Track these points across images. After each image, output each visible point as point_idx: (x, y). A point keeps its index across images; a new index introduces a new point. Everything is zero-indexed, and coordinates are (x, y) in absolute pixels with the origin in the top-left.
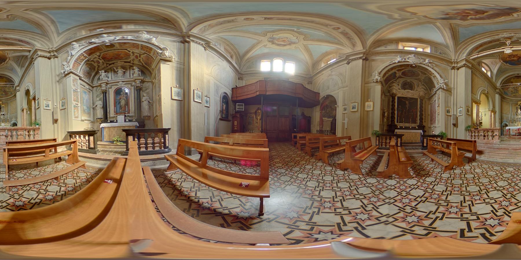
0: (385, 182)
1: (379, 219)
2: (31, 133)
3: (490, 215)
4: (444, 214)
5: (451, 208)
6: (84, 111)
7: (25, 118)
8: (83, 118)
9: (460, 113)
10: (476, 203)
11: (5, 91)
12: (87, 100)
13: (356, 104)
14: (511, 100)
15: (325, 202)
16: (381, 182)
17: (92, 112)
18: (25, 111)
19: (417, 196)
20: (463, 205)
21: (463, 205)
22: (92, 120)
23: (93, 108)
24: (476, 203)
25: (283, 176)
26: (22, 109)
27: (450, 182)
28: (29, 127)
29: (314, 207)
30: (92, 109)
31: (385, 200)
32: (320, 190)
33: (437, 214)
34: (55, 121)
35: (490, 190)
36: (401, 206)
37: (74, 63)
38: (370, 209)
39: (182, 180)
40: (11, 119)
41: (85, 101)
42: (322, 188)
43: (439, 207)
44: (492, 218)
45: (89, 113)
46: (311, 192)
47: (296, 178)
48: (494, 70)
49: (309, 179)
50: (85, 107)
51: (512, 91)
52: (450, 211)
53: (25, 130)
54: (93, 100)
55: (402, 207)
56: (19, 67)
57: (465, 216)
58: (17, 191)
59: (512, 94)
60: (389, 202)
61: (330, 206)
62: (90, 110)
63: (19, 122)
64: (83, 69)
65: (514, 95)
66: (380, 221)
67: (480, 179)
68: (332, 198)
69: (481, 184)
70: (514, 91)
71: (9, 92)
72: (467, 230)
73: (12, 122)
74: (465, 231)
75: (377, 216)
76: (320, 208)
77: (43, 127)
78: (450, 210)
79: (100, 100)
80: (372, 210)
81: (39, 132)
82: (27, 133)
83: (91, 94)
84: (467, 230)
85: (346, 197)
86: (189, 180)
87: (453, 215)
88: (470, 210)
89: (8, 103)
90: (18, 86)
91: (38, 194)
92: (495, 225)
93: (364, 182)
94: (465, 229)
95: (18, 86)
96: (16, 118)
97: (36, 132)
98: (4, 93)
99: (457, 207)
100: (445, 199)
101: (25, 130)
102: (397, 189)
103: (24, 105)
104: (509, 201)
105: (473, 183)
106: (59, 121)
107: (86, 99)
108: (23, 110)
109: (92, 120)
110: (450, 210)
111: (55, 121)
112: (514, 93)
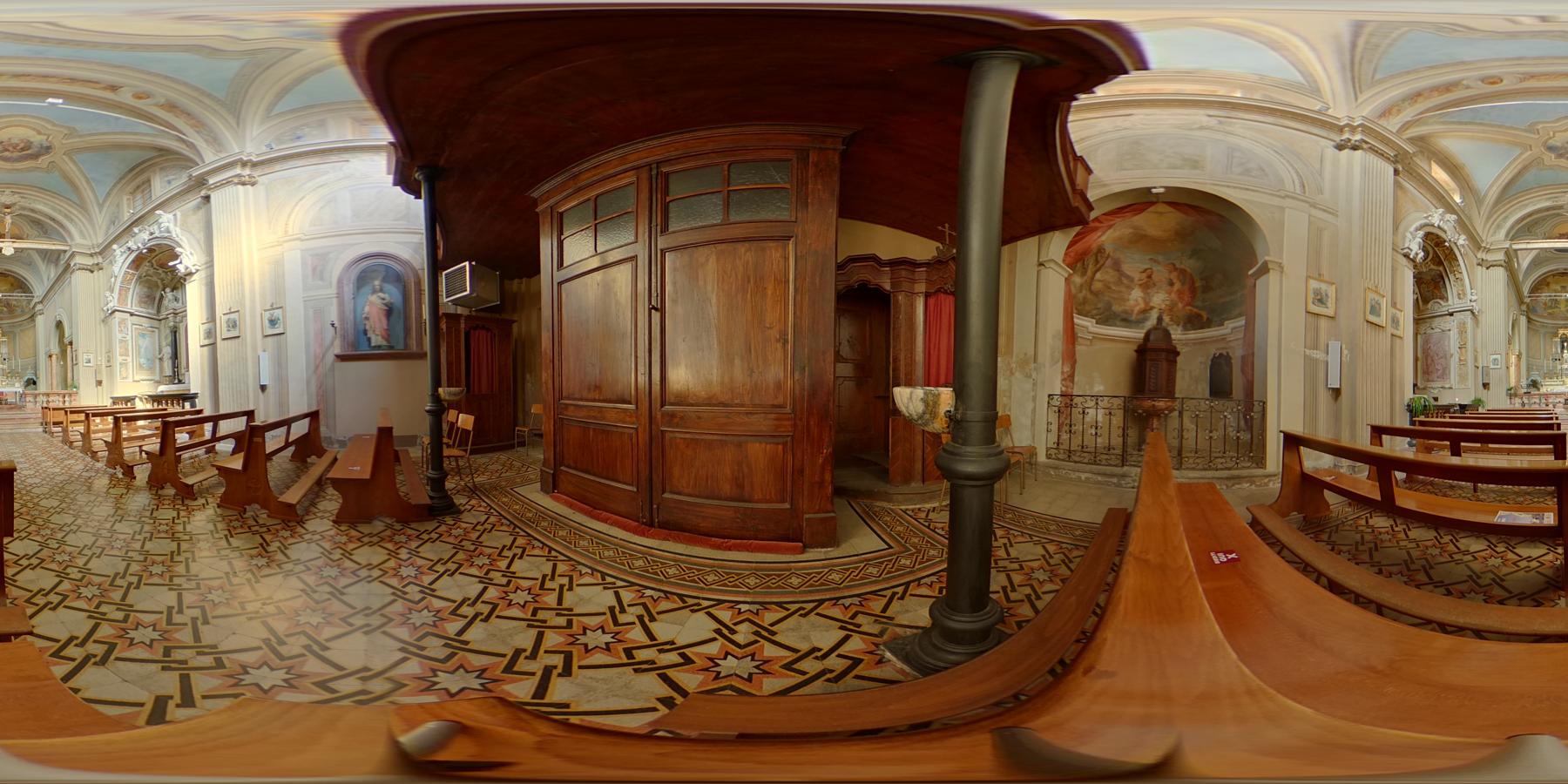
0: (1511, 548)
1: (332, 685)
2: (67, 398)
3: (260, 653)
4: (112, 647)
5: (136, 629)
6: (141, 366)
7: (54, 371)
8: (137, 378)
9: (1494, 365)
10: (603, 617)
11: (8, 304)
12: (146, 348)
13: (1498, 357)
14: (1544, 325)
15: (585, 629)
16: (1501, 548)
17: (158, 366)
18: (54, 357)
19: (459, 599)
20: (174, 621)
21: (174, 621)
22: (157, 378)
23: (160, 359)
24: (602, 618)
25: (428, 544)
26: (49, 354)
27: (133, 564)
28: (63, 392)
29: (546, 652)
30: (157, 361)
31: (385, 620)
32: (562, 587)
33: (91, 648)
34: (99, 383)
35: (1467, 585)
36: (767, 644)
37: (120, 290)
38: (297, 650)
39: (515, 550)
40: (25, 369)
41: (142, 350)
42: (565, 581)
43: (100, 624)
44: (265, 663)
45: (151, 369)
46: (529, 598)
47: (473, 547)
48: (1523, 261)
49: (519, 551)
50: (142, 361)
51: (1545, 304)
52: (132, 639)
53: (59, 395)
54: (159, 346)
55: (411, 641)
56: (44, 262)
57: (178, 655)
58: (410, 609)
59: (1545, 309)
60: (368, 625)
61: (152, 641)
62: (153, 361)
63: (41, 378)
64: (137, 293)
65: (1550, 314)
66: (333, 691)
67: (1011, 546)
68: (608, 614)
69: (1016, 566)
70: (1550, 304)
71: (18, 307)
72: (179, 702)
73: (26, 378)
74: (170, 702)
75: (326, 674)
76: (571, 652)
77: (82, 391)
78: (132, 634)
79: (167, 345)
80: (303, 655)
81: (77, 398)
82: (61, 399)
83: (157, 334)
84: (179, 702)
85: (655, 608)
86: (536, 552)
87: (140, 650)
88: (197, 638)
89: (15, 334)
90: (41, 302)
91: (93, 622)
92: (462, 690)
93: (1451, 547)
94: (171, 697)
95: (41, 302)
96: (35, 368)
97: (73, 398)
98: (5, 309)
99: (154, 625)
100: (878, 612)
101: (59, 395)
102: (389, 577)
103: (52, 347)
104: (740, 613)
105: (1427, 549)
106: (104, 383)
107: (144, 346)
108: (50, 356)
109: (157, 378)
110: (132, 634)
111: (99, 383)
112: (1551, 307)
